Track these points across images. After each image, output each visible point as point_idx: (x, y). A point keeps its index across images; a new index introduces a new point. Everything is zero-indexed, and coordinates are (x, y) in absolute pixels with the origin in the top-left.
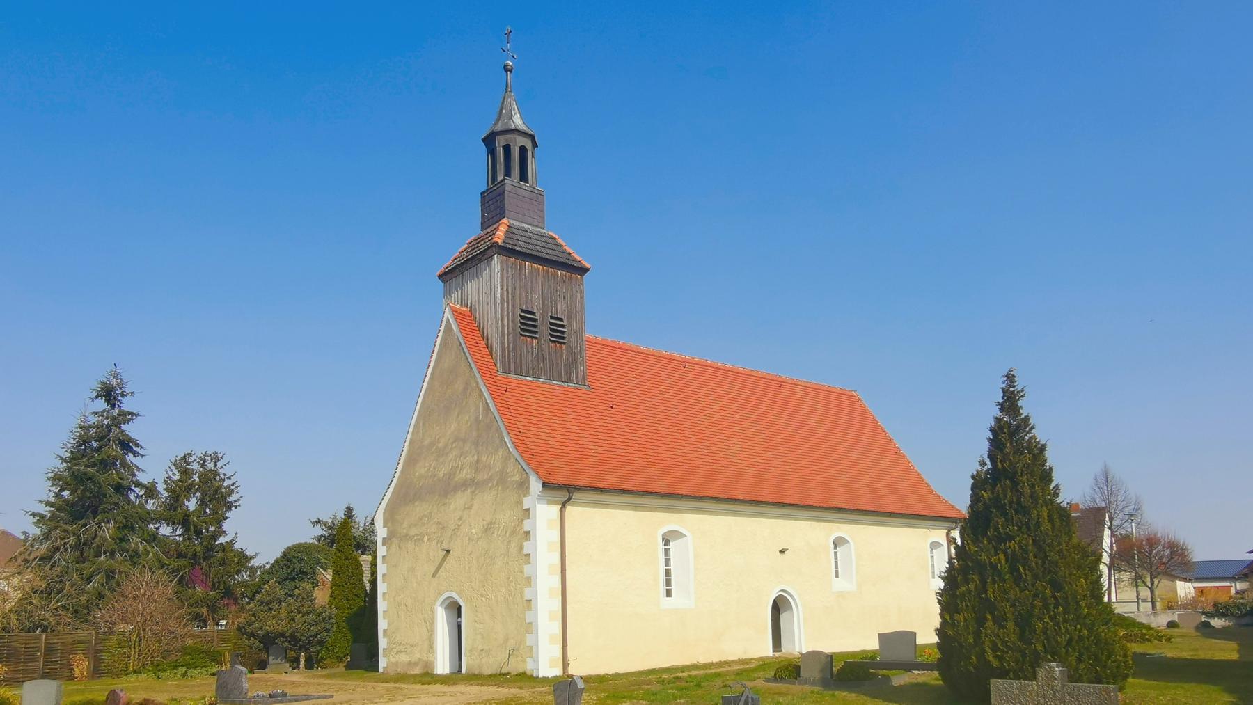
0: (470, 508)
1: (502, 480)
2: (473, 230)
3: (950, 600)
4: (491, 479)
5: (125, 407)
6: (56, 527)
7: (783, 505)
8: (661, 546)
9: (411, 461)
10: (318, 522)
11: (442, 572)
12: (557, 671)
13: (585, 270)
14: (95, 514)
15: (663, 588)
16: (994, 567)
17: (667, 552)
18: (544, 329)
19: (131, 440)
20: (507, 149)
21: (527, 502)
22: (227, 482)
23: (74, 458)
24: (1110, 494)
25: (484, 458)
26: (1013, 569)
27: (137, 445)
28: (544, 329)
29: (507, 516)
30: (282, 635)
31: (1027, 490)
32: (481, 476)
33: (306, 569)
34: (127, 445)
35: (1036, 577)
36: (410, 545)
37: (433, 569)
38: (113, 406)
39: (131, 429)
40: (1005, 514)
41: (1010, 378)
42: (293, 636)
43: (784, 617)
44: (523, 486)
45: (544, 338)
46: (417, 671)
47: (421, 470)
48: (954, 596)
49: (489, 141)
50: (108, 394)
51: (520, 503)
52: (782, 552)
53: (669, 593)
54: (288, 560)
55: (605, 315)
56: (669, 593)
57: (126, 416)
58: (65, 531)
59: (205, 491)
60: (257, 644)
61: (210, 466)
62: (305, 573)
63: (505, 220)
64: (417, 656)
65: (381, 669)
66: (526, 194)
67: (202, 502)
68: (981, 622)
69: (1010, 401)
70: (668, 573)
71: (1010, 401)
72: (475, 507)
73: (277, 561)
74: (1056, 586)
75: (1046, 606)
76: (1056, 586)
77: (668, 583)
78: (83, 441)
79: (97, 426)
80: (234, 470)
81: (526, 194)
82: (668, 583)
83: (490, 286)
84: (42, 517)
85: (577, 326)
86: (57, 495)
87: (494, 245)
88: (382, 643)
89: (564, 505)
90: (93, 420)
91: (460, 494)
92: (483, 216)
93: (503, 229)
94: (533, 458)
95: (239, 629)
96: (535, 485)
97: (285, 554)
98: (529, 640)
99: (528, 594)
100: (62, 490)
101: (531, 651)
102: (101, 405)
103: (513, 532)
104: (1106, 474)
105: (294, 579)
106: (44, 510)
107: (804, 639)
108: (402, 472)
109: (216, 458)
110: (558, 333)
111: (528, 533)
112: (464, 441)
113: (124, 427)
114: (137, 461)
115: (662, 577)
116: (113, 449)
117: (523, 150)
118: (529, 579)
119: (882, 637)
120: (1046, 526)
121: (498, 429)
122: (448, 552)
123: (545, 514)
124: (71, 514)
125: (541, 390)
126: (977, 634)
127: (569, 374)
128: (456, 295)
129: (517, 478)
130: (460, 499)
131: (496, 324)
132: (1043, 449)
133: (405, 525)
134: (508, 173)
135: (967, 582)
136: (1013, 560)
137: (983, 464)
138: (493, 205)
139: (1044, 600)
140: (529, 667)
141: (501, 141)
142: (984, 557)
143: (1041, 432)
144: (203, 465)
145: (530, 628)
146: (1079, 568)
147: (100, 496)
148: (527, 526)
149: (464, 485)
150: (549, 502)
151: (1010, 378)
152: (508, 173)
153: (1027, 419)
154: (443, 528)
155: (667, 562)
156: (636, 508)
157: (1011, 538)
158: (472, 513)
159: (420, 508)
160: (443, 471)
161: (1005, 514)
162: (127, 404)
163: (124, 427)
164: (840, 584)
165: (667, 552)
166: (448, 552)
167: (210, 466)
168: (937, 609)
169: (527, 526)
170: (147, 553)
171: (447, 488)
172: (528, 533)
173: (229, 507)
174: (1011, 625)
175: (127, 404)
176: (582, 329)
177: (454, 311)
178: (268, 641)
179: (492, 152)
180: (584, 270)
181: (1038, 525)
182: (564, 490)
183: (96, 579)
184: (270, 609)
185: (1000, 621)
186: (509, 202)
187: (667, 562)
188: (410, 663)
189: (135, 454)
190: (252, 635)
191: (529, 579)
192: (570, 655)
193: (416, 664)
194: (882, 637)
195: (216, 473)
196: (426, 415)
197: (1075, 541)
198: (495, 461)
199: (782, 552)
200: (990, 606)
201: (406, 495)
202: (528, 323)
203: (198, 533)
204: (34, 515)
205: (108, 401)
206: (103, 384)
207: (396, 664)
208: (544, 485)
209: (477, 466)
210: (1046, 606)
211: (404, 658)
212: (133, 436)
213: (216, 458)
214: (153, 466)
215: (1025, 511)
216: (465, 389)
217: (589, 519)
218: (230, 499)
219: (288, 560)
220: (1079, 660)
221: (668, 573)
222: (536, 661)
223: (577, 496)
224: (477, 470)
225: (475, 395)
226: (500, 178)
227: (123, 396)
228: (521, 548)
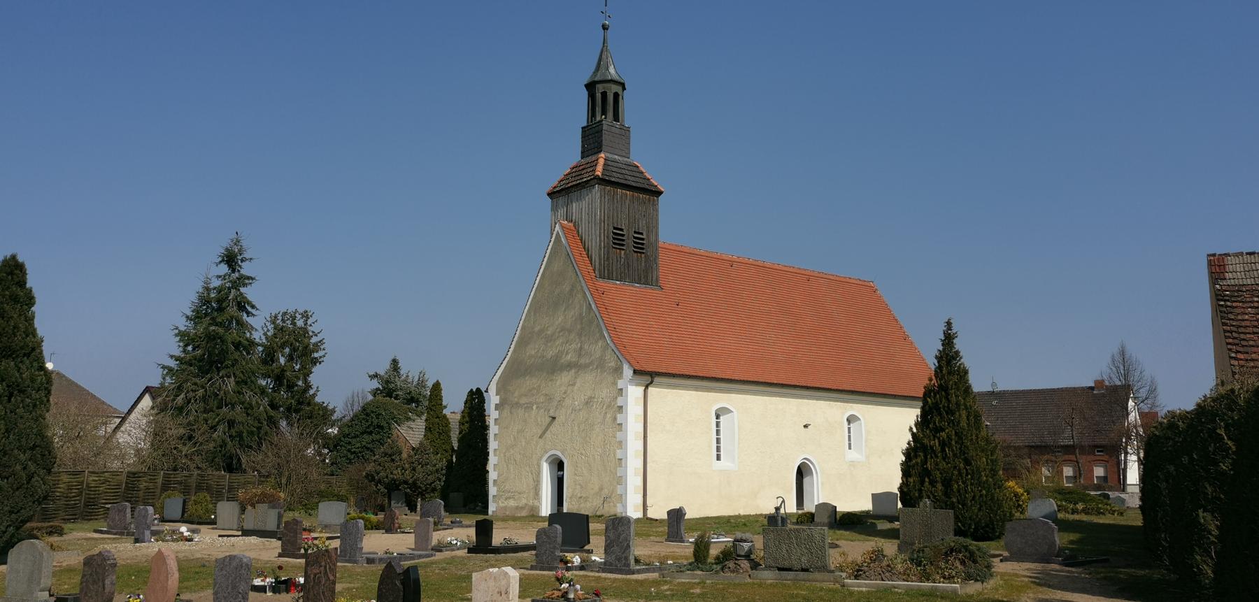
0: (574, 385)
1: (601, 365)
2: (573, 156)
3: (907, 469)
4: (591, 363)
5: (242, 272)
6: (187, 381)
7: (807, 388)
8: (714, 420)
9: (523, 343)
10: (376, 376)
11: (548, 434)
12: (639, 515)
13: (659, 193)
14: (218, 370)
15: (715, 453)
16: (932, 447)
17: (718, 425)
18: (629, 242)
19: (249, 303)
20: (604, 95)
21: (620, 384)
22: (314, 340)
23: (197, 317)
24: (1126, 376)
25: (586, 347)
26: (943, 450)
27: (253, 307)
28: (629, 242)
29: (604, 393)
30: (406, 482)
31: (954, 399)
32: (582, 361)
33: (384, 424)
34: (243, 305)
35: (955, 455)
36: (521, 412)
37: (540, 432)
38: (234, 271)
39: (249, 292)
40: (940, 414)
41: (949, 324)
42: (414, 483)
43: (806, 480)
44: (618, 371)
45: (629, 253)
46: (524, 513)
47: (531, 350)
48: (909, 467)
49: (590, 86)
50: (231, 259)
51: (615, 384)
52: (806, 426)
53: (718, 458)
54: (367, 415)
55: (674, 226)
56: (718, 458)
57: (244, 280)
58: (195, 384)
59: (297, 344)
60: (383, 489)
61: (300, 323)
62: (382, 427)
63: (602, 155)
64: (524, 501)
65: (490, 512)
66: (617, 131)
67: (290, 358)
68: (922, 483)
69: (948, 339)
70: (718, 441)
71: (948, 339)
72: (578, 384)
73: (356, 416)
74: (967, 462)
75: (960, 474)
76: (967, 462)
77: (718, 449)
78: (205, 301)
79: (219, 290)
80: (323, 328)
81: (617, 131)
82: (718, 449)
83: (592, 203)
84: (170, 370)
85: (653, 238)
86: (184, 351)
87: (597, 178)
88: (492, 490)
89: (647, 387)
90: (216, 283)
91: (565, 373)
92: (583, 146)
93: (601, 161)
94: (623, 352)
95: (367, 476)
96: (628, 372)
97: (364, 409)
98: (619, 490)
99: (619, 454)
100: (186, 345)
101: (622, 498)
102: (224, 269)
103: (609, 406)
104: (1123, 353)
105: (371, 433)
106: (173, 364)
107: (821, 493)
108: (514, 351)
109: (306, 316)
110: (639, 246)
111: (621, 407)
112: (570, 331)
113: (242, 290)
114: (250, 320)
115: (714, 445)
116: (232, 310)
117: (616, 96)
118: (621, 442)
119: (875, 497)
120: (964, 424)
121: (598, 325)
122: (554, 418)
123: (634, 392)
124: (200, 368)
125: (623, 293)
126: (920, 491)
127: (646, 277)
128: (562, 212)
129: (613, 364)
130: (565, 378)
131: (596, 239)
132: (966, 372)
133: (516, 394)
134: (604, 112)
135: (916, 456)
136: (943, 444)
137: (931, 380)
138: (592, 140)
139: (959, 470)
140: (619, 510)
141: (600, 88)
142: (926, 441)
143: (967, 360)
144: (294, 324)
145: (621, 481)
146: (983, 451)
147: (224, 353)
148: (620, 401)
149: (570, 366)
150: (637, 385)
151: (949, 324)
152: (604, 112)
153: (957, 353)
154: (550, 399)
155: (718, 432)
156: (697, 389)
157: (943, 430)
158: (580, 388)
159: (529, 382)
160: (550, 353)
161: (940, 414)
162: (246, 269)
163: (242, 290)
164: (852, 455)
165: (718, 425)
166: (554, 418)
167: (300, 323)
168: (900, 474)
169: (620, 401)
170: (258, 405)
171: (553, 367)
172: (621, 407)
173: (315, 362)
174: (939, 486)
175: (246, 269)
176: (657, 240)
177: (562, 227)
178: (393, 487)
179: (592, 96)
180: (659, 193)
181: (959, 422)
182: (648, 376)
183: (221, 428)
184: (393, 460)
185: (932, 483)
186: (606, 138)
187: (718, 432)
188: (517, 508)
189: (248, 313)
190: (379, 481)
191: (621, 442)
192: (649, 503)
193: (522, 508)
194: (875, 497)
195: (305, 331)
196: (536, 308)
197: (984, 433)
198: (596, 349)
199: (806, 426)
200: (927, 473)
201: (516, 371)
202: (618, 239)
203: (290, 387)
204: (164, 367)
205: (230, 266)
206: (227, 249)
207: (505, 508)
208: (635, 372)
209: (580, 352)
210: (960, 474)
211: (512, 503)
212: (250, 298)
213: (306, 316)
214: (259, 327)
215: (950, 412)
216: (571, 290)
217: (666, 399)
218: (316, 355)
219: (367, 415)
220: (980, 510)
221: (718, 441)
222: (625, 507)
223: (657, 379)
224: (580, 355)
225: (580, 296)
226: (598, 119)
227: (242, 261)
228: (615, 419)
